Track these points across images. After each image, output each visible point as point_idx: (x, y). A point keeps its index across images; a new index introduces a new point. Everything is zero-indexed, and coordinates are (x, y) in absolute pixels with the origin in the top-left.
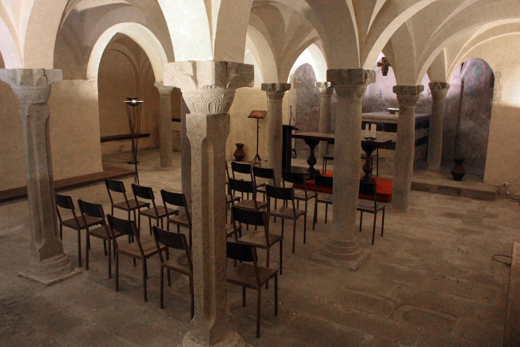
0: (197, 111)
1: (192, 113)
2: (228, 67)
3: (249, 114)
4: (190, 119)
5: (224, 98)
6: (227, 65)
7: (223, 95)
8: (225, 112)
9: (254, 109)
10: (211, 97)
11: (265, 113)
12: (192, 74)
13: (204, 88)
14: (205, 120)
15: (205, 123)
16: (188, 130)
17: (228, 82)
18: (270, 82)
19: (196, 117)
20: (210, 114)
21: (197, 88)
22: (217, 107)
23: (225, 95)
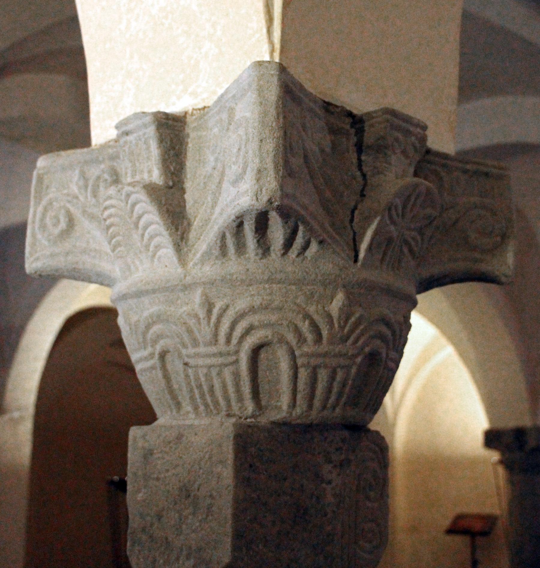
0: (187, 407)
1: (163, 419)
2: (369, 138)
3: (447, 523)
4: (148, 454)
5: (346, 314)
6: (360, 132)
7: (339, 299)
8: (352, 414)
9: (459, 510)
10: (265, 308)
11: (489, 521)
12: (156, 176)
13: (223, 248)
15: (227, 474)
16: (135, 522)
17: (368, 220)
18: (510, 423)
21: (182, 260)
22: (303, 374)
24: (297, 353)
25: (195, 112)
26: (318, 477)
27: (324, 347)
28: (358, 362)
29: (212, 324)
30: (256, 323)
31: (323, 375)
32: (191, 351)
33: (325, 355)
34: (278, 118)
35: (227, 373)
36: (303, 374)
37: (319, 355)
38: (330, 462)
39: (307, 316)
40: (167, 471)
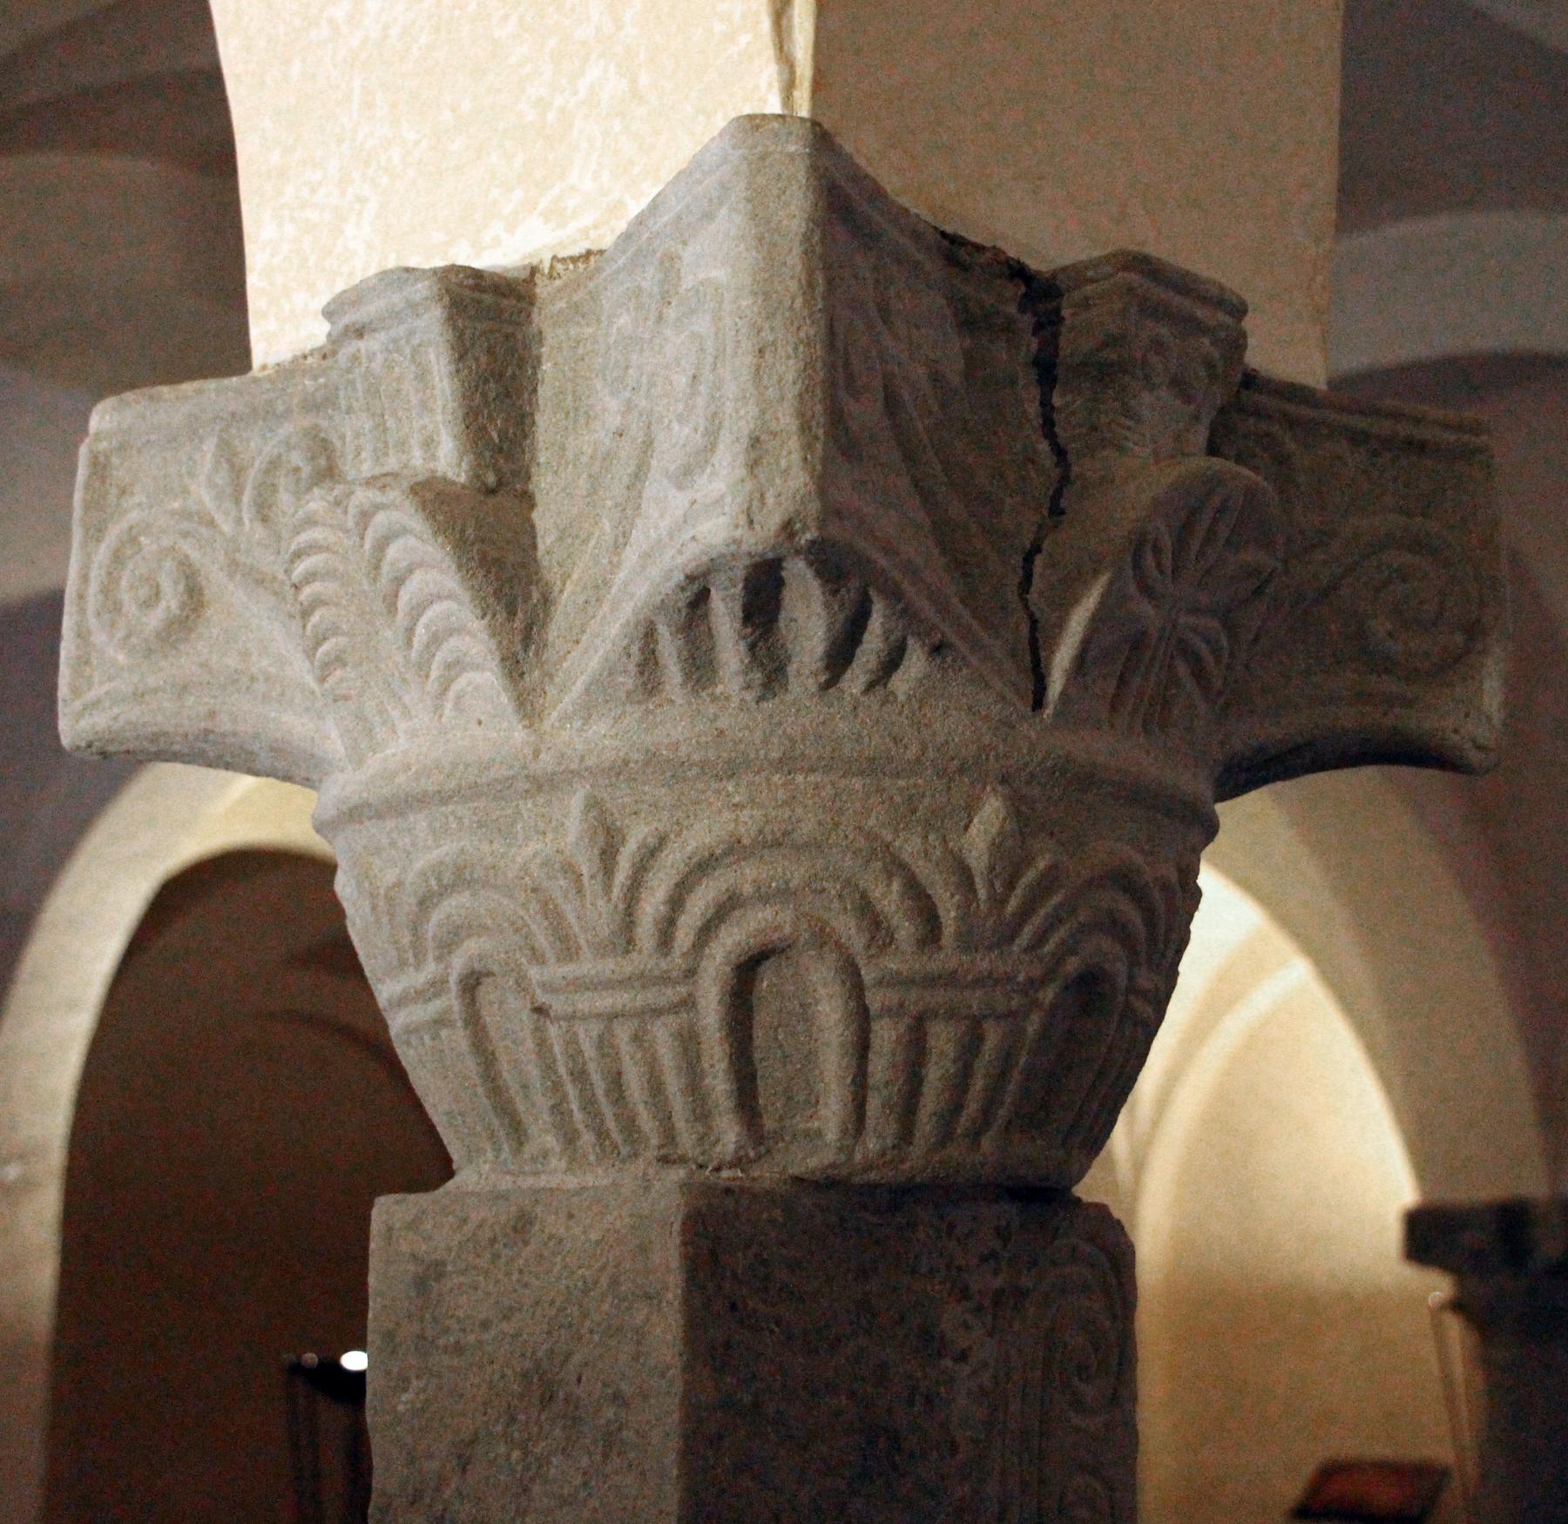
2: (1073, 345)
4: (428, 1276)
5: (1010, 860)
6: (1048, 324)
7: (991, 814)
12: (448, 458)
13: (649, 662)
14: (668, 1256)
15: (665, 1331)
17: (1064, 604)
18: (1481, 1188)
19: (522, 1225)
20: (766, 1174)
21: (527, 705)
22: (885, 1035)
23: (1025, 819)
24: (868, 975)
25: (559, 267)
26: (930, 1342)
27: (947, 957)
28: (1047, 1002)
29: (616, 892)
30: (748, 889)
31: (943, 1040)
32: (559, 971)
33: (950, 979)
34: (811, 285)
35: (662, 1035)
36: (885, 1035)
37: (931, 981)
38: (965, 1294)
39: (896, 866)
40: (485, 1325)
